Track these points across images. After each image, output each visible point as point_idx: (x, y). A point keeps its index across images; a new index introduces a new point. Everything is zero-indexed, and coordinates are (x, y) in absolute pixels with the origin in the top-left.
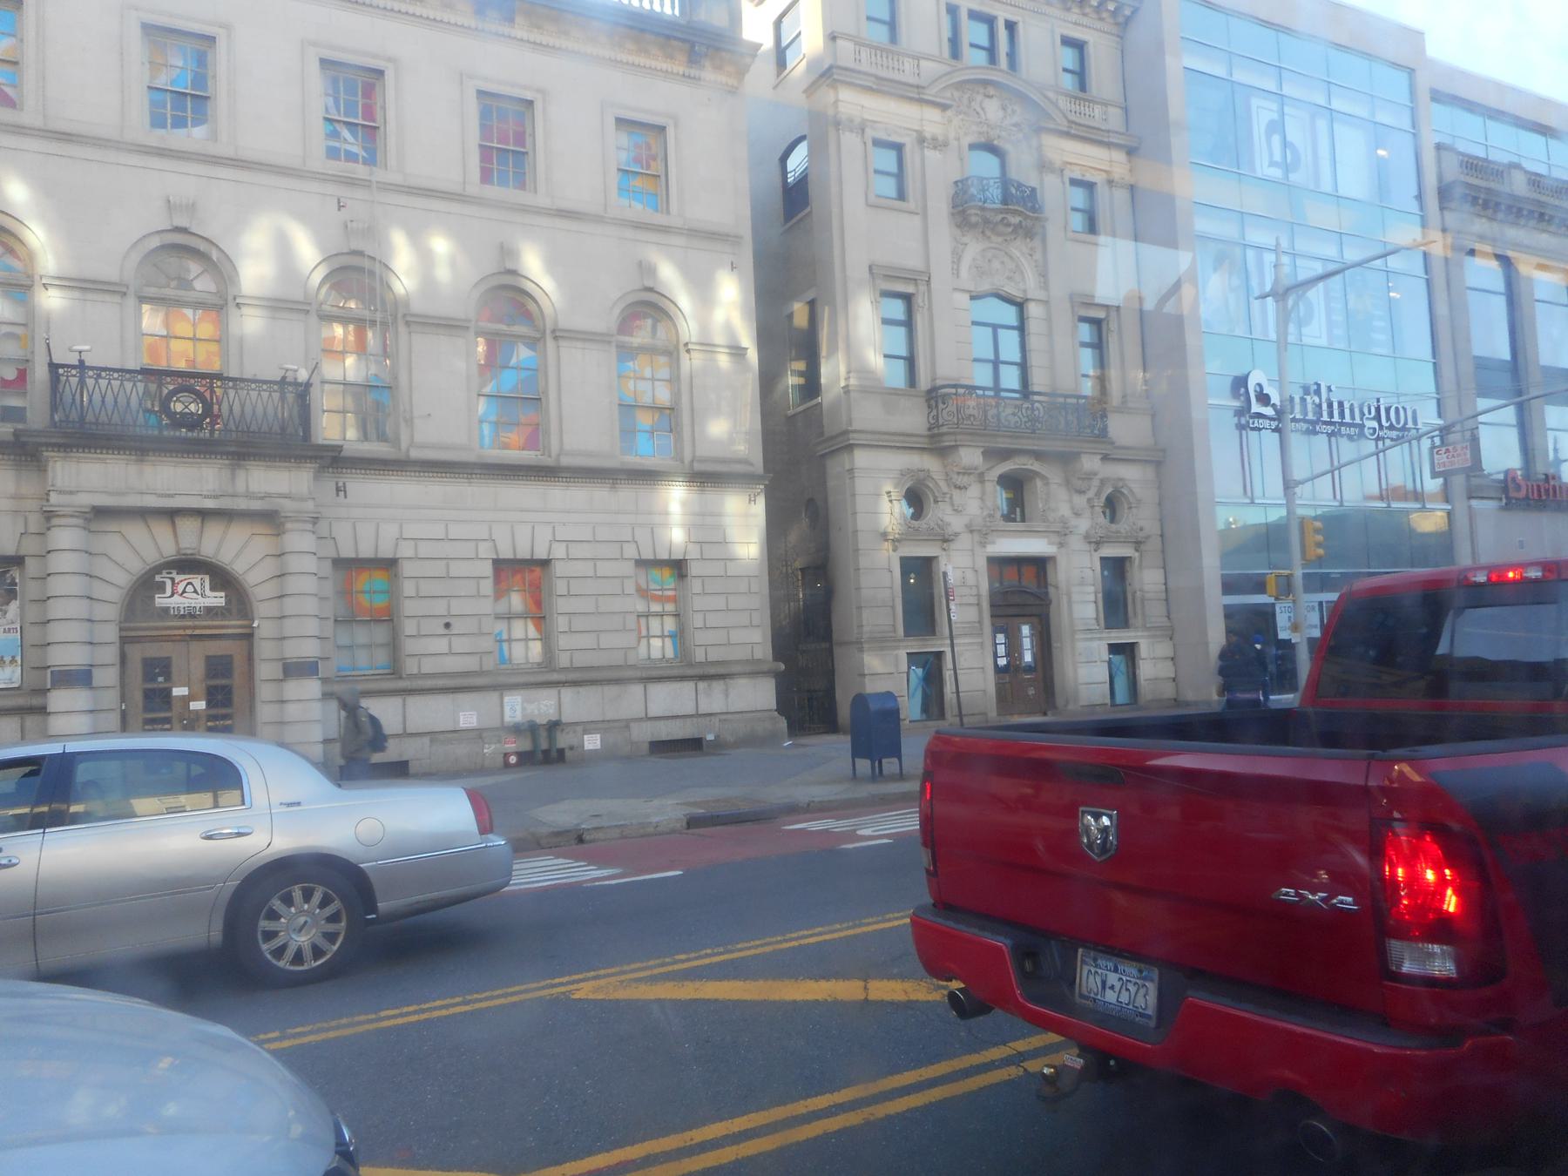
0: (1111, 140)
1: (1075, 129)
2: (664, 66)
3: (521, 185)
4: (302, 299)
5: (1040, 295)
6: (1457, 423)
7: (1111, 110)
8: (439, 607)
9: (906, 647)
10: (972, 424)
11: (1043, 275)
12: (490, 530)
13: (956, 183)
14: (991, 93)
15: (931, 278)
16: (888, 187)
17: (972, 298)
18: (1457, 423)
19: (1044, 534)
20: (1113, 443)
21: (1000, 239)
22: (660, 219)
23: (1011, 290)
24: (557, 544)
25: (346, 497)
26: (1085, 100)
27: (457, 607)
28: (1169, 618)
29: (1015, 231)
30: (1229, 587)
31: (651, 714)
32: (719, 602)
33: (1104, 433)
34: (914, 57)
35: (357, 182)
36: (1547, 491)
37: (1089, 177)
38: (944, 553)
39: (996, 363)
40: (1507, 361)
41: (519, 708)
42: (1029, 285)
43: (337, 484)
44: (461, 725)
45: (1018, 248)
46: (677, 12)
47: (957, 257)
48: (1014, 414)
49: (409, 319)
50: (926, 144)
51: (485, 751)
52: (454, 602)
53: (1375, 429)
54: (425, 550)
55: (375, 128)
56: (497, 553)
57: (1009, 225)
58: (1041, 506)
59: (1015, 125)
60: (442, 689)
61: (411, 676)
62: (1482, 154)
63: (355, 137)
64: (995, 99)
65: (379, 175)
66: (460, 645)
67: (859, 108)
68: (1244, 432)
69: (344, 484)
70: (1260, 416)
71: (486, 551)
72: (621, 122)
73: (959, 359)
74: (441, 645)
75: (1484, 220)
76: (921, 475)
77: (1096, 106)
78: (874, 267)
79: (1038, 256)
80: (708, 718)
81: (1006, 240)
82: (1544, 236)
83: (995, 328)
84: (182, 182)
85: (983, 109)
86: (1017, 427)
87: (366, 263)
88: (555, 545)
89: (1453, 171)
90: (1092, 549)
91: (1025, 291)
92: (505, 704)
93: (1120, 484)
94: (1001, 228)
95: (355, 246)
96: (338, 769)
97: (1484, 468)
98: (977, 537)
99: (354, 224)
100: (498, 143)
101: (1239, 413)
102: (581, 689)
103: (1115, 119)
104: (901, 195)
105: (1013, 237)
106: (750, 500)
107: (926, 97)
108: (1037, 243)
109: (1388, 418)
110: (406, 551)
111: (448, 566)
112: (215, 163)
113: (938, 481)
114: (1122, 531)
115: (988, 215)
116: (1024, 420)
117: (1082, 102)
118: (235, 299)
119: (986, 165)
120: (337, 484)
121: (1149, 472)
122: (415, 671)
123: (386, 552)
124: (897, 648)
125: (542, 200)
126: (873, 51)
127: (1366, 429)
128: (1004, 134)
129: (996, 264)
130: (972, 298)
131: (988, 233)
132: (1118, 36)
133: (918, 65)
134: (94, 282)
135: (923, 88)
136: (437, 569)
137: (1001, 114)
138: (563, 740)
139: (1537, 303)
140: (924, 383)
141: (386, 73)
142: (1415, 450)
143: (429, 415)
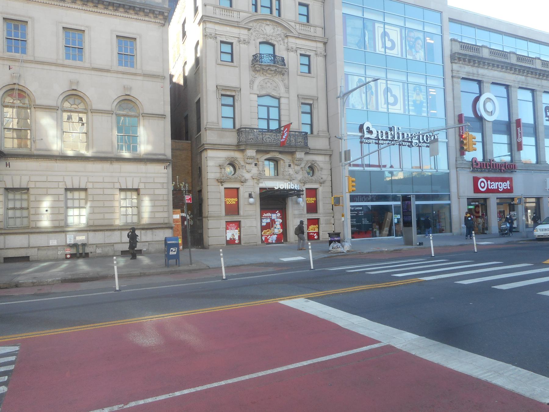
0: (316, 39)
1: (301, 36)
2: (135, 17)
3: (132, 66)
4: (110, 110)
5: (287, 95)
7: (318, 29)
9: (225, 219)
10: (252, 142)
11: (287, 88)
12: (64, 178)
13: (253, 56)
14: (268, 24)
15: (318, 99)
16: (306, 69)
17: (258, 96)
19: (283, 180)
20: (310, 148)
21: (270, 76)
22: (132, 70)
23: (274, 93)
24: (142, 184)
25: (9, 167)
26: (309, 26)
28: (333, 210)
29: (275, 73)
30: (353, 199)
31: (123, 241)
33: (306, 145)
34: (237, 11)
35: (16, 60)
36: (490, 166)
37: (308, 53)
38: (242, 186)
39: (268, 120)
40: (532, 124)
41: (72, 239)
42: (282, 91)
43: (6, 163)
44: (51, 244)
45: (278, 79)
47: (252, 82)
48: (269, 138)
49: (143, 115)
50: (241, 42)
51: (59, 253)
53: (417, 143)
54: (38, 185)
55: (133, 56)
56: (66, 186)
57: (272, 71)
58: (282, 170)
59: (278, 35)
60: (38, 232)
61: (33, 228)
62: (526, 55)
64: (270, 26)
65: (25, 57)
67: (215, 30)
68: (400, 146)
69: (9, 163)
70: (369, 138)
71: (62, 186)
73: (251, 118)
75: (470, 67)
76: (232, 159)
77: (311, 27)
78: (218, 86)
79: (286, 82)
80: (144, 243)
81: (272, 76)
82: (496, 72)
83: (268, 107)
84: (127, 81)
85: (265, 29)
86: (270, 143)
88: (88, 184)
89: (457, 48)
90: (302, 185)
91: (280, 94)
92: (67, 237)
93: (313, 163)
94: (269, 71)
96: (120, 252)
97: (546, 161)
98: (255, 181)
99: (14, 75)
100: (14, 37)
101: (362, 137)
102: (96, 233)
103: (319, 33)
104: (309, 72)
105: (275, 75)
106: (165, 168)
107: (240, 26)
108: (286, 77)
109: (423, 139)
110: (31, 185)
111: (154, 191)
113: (240, 162)
114: (314, 179)
115: (263, 67)
116: (273, 140)
117: (302, 25)
118: (142, 114)
119: (267, 50)
120: (6, 163)
121: (327, 158)
122: (34, 226)
123: (24, 186)
124: (221, 219)
125: (87, 65)
126: (221, 10)
127: (413, 143)
128: (273, 38)
129: (269, 84)
130: (258, 96)
131: (265, 73)
132: (322, 2)
133: (239, 14)
134: (105, 111)
135: (239, 22)
137: (272, 31)
138: (88, 250)
139: (518, 101)
140: (238, 127)
141: (28, 22)
142: (420, 149)
143: (42, 139)
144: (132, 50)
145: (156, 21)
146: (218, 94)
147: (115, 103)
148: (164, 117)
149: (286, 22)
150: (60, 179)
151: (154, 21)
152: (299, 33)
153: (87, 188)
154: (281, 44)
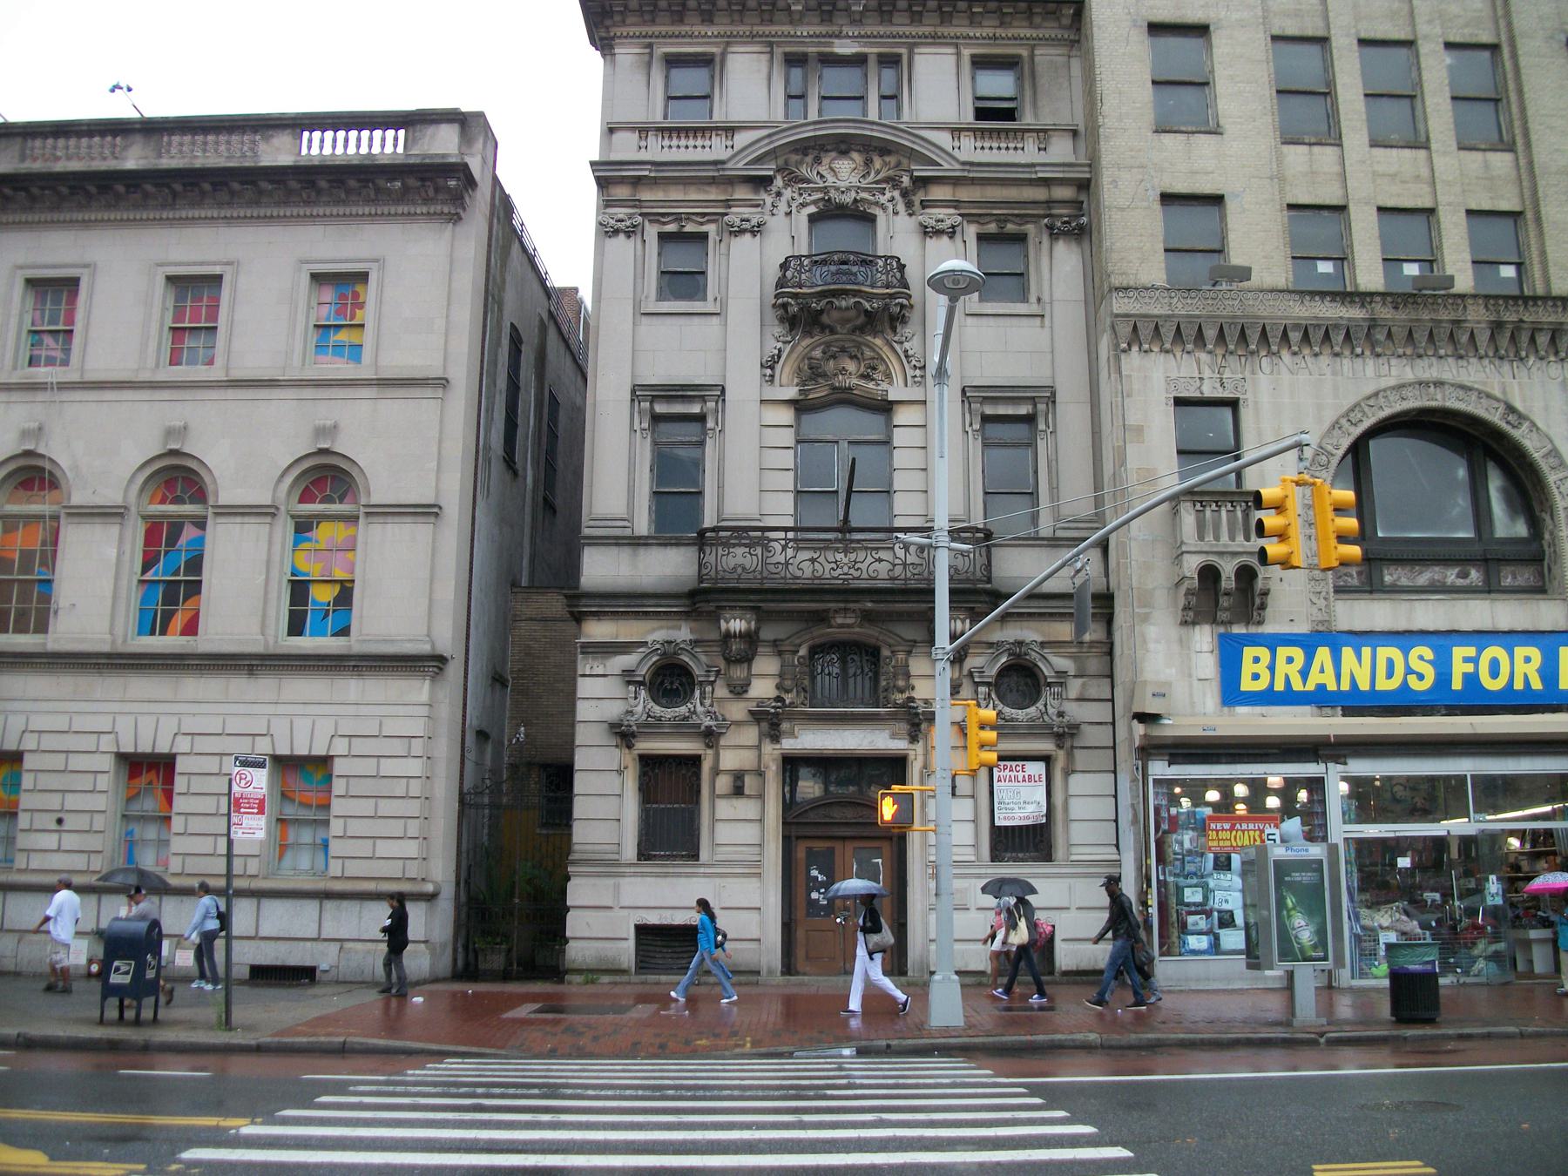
4: (269, 503)
6: (1535, 524)
8: (54, 802)
18: (1535, 524)
27: (72, 802)
32: (366, 807)
46: (400, 149)
52: (69, 797)
54: (49, 742)
63: (57, 342)
66: (70, 841)
72: (317, 278)
74: (50, 841)
87: (40, 463)
95: (29, 446)
110: (29, 743)
112: (102, 388)
123: (319, 750)
135: (723, 162)
136: (57, 762)
144: (70, 319)
145: (432, 211)
146: (970, 413)
147: (289, 479)
148: (436, 510)
149: (910, 133)
150: (103, 723)
151: (425, 210)
152: (964, 163)
153: (174, 751)
154: (896, 213)
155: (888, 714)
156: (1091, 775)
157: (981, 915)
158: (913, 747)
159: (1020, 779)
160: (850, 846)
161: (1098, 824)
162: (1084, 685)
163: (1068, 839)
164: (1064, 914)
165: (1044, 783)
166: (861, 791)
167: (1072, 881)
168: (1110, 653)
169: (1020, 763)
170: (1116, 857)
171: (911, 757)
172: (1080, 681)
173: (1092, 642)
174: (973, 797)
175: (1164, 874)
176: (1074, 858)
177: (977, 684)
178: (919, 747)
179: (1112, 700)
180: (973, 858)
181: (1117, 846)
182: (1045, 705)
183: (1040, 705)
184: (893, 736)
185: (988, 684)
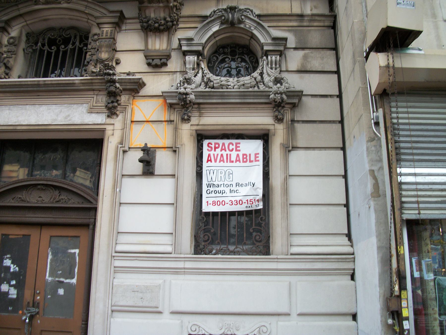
155: (83, 83)
156: (316, 152)
157: (176, 321)
158: (109, 121)
159: (234, 158)
160: (47, 233)
161: (324, 208)
162: (305, 57)
163: (288, 227)
164: (282, 322)
165: (261, 163)
166: (64, 176)
167: (294, 279)
168: (334, 27)
169: (234, 141)
170: (348, 249)
171: (108, 132)
172: (301, 53)
173: (313, 15)
174: (173, 176)
175: (420, 270)
176: (295, 250)
177: (185, 53)
178: (118, 122)
179: (338, 72)
180: (169, 249)
181: (349, 236)
182: (261, 74)
183: (256, 74)
184: (91, 111)
185: (198, 54)
